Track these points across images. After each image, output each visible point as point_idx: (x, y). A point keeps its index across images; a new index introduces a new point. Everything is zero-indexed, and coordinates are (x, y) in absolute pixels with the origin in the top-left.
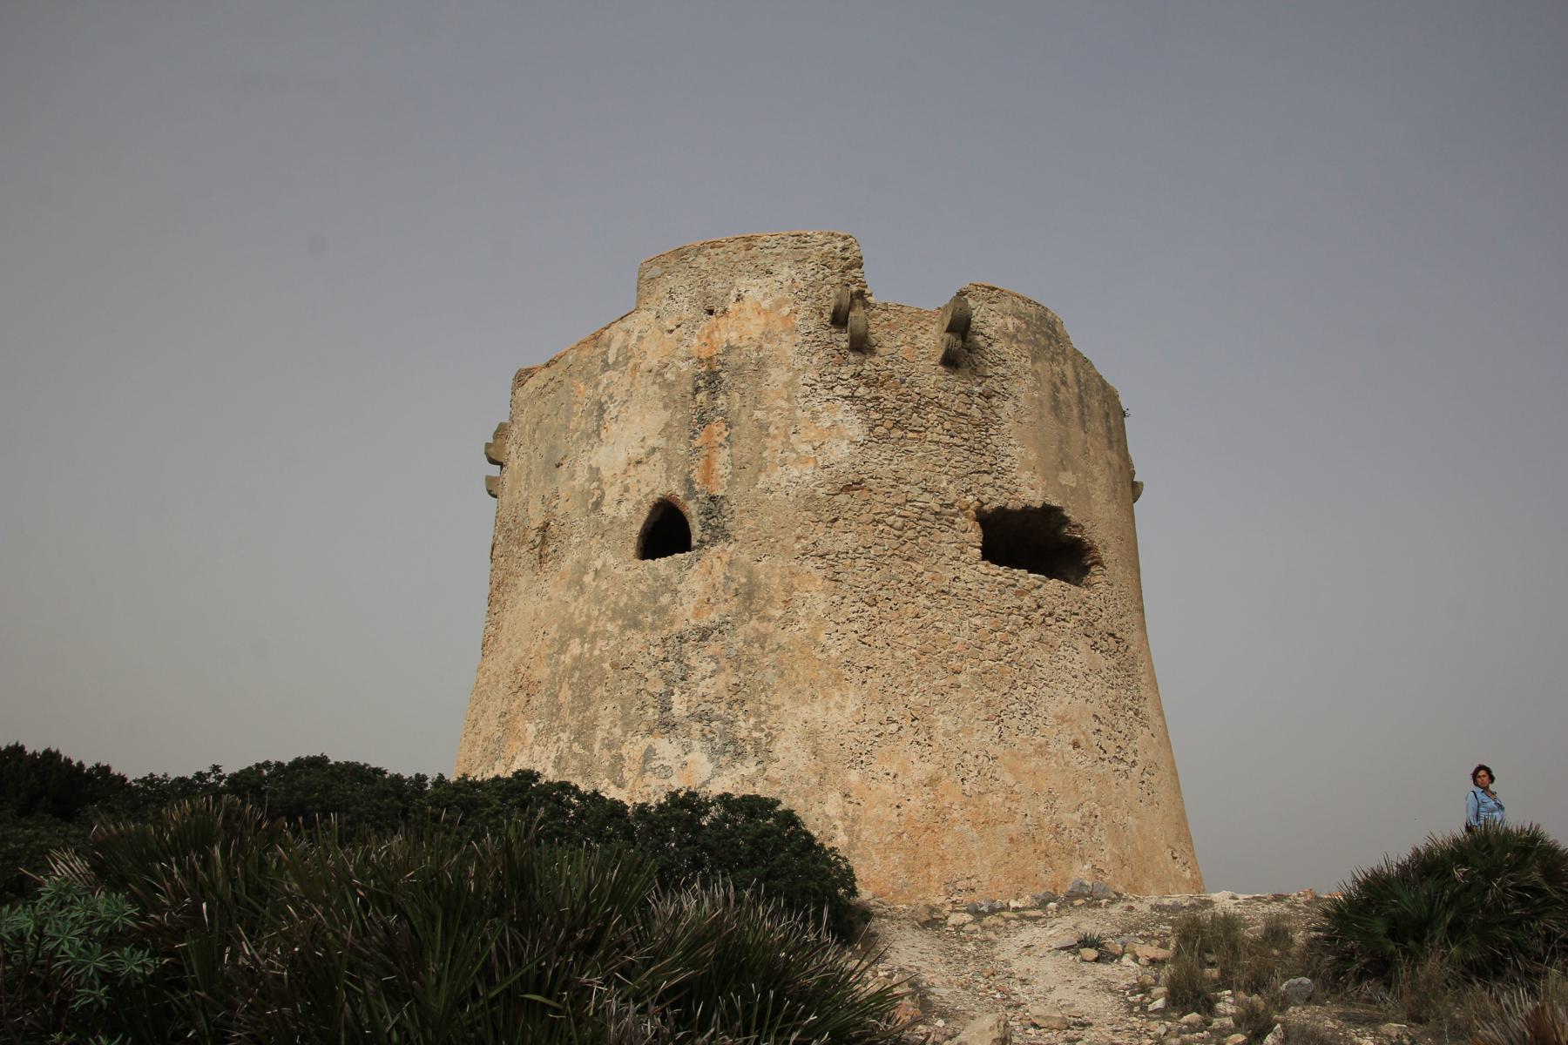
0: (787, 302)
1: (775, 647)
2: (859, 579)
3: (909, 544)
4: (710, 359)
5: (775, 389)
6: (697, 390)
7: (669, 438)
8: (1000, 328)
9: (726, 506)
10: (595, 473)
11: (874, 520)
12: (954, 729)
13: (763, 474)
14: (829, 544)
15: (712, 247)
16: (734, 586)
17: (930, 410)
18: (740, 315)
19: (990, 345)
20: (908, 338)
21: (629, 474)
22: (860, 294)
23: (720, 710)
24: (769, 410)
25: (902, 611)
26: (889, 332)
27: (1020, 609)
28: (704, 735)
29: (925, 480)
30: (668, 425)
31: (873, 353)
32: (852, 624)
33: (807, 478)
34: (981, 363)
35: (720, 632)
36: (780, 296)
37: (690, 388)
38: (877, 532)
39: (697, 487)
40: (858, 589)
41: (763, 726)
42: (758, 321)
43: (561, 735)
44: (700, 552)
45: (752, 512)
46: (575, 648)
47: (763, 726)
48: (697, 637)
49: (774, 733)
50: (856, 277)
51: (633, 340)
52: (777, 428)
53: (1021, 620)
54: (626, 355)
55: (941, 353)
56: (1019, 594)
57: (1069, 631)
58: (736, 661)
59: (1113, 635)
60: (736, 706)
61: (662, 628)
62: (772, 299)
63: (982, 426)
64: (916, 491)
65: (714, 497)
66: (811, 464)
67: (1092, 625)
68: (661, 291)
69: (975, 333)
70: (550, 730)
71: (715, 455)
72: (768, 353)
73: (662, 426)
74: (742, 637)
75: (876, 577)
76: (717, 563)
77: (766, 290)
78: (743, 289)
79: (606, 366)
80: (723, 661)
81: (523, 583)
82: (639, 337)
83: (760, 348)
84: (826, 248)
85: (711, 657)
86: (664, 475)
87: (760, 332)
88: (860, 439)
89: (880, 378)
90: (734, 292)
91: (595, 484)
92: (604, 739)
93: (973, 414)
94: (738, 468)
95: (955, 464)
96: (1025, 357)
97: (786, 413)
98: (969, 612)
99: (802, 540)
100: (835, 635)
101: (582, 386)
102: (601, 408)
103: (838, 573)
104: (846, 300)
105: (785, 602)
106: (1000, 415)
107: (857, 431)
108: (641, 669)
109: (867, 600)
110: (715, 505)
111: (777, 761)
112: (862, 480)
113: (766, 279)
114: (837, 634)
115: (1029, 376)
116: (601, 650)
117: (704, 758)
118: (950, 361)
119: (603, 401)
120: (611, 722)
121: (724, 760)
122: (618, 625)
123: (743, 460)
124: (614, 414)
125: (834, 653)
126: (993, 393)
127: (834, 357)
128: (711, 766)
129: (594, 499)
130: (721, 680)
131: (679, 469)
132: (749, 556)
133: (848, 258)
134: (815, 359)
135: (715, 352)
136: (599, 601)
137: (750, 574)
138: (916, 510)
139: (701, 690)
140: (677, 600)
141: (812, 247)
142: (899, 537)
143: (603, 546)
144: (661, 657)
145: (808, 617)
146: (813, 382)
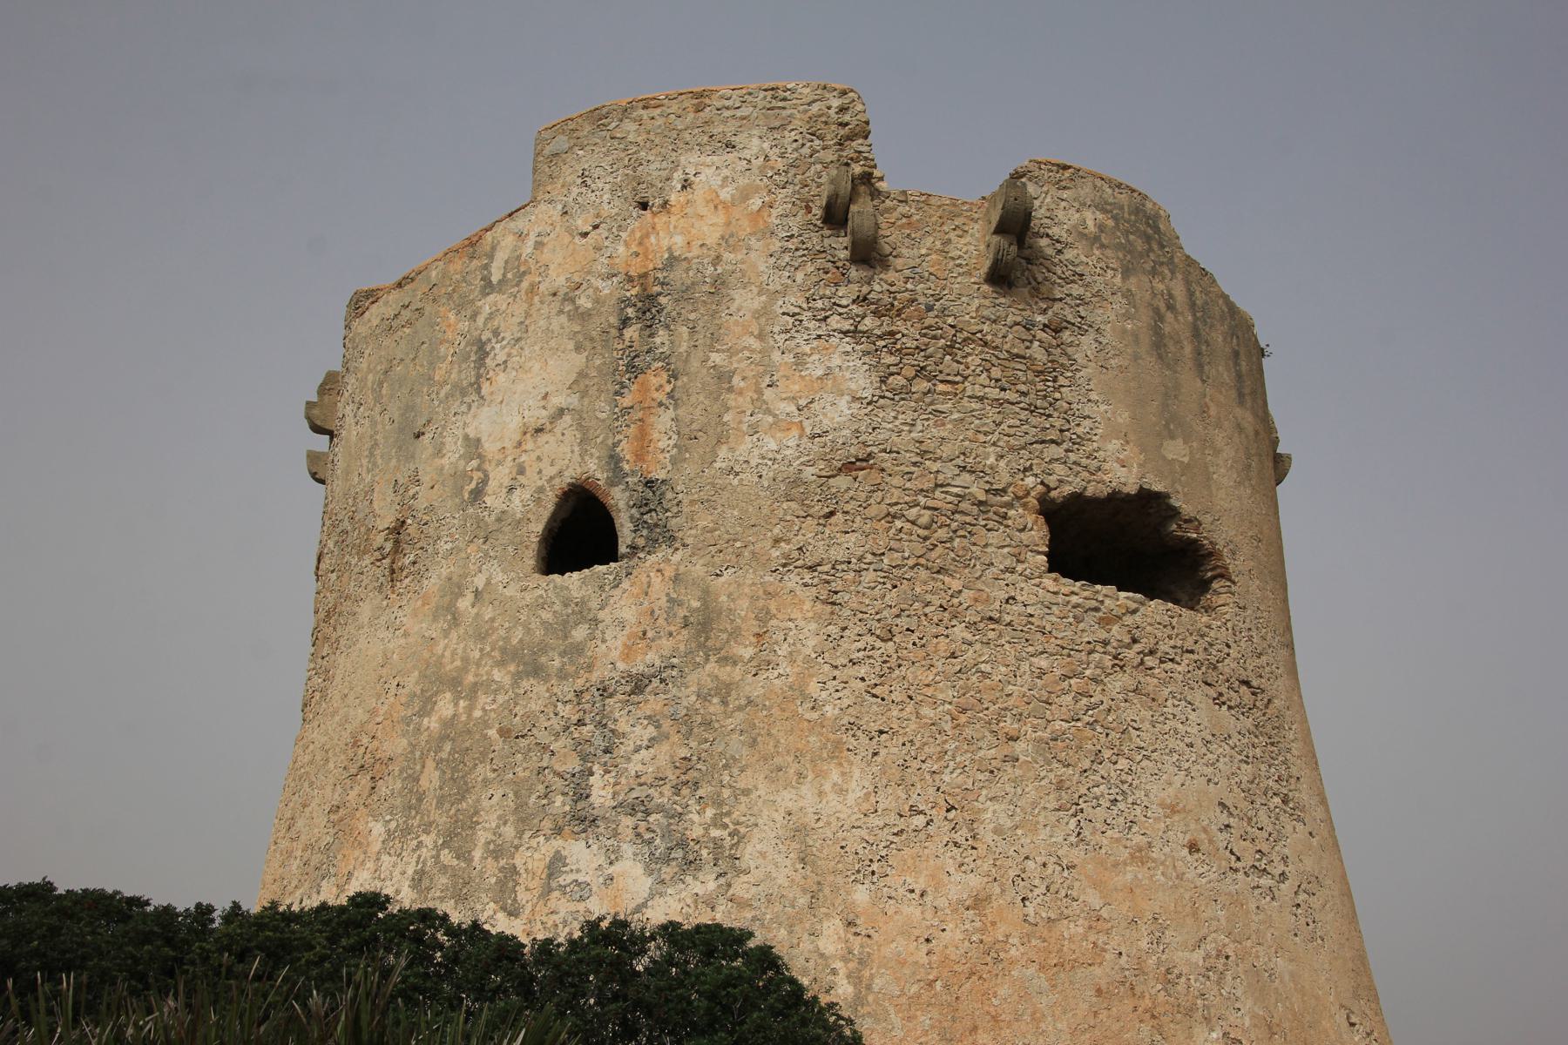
0: (757, 190)
3: (939, 550)
4: (645, 276)
5: (741, 320)
7: (584, 394)
8: (1074, 226)
9: (669, 495)
10: (473, 446)
12: (1009, 824)
13: (724, 447)
15: (645, 107)
16: (682, 612)
18: (687, 210)
19: (1060, 252)
20: (938, 243)
21: (524, 447)
22: (867, 178)
23: (663, 796)
24: (732, 352)
25: (930, 648)
28: (638, 835)
29: (964, 454)
30: (582, 375)
31: (886, 266)
32: (856, 667)
33: (788, 452)
34: (1046, 279)
36: (747, 181)
37: (614, 320)
38: (893, 531)
39: (626, 467)
40: (865, 616)
41: (726, 820)
42: (715, 220)
46: (445, 706)
47: (726, 820)
48: (628, 689)
49: (743, 830)
50: (860, 152)
51: (528, 248)
53: (1108, 661)
54: (518, 270)
55: (987, 264)
56: (1105, 622)
58: (686, 724)
59: (1247, 683)
60: (685, 791)
61: (576, 675)
62: (735, 185)
65: (653, 482)
66: (795, 432)
68: (569, 174)
69: (1038, 235)
70: (406, 831)
72: (729, 267)
73: (573, 377)
74: (695, 688)
75: (892, 596)
76: (657, 580)
77: (726, 172)
79: (488, 287)
80: (666, 725)
84: (815, 108)
86: (576, 449)
87: (718, 235)
88: (867, 394)
89: (896, 303)
90: (678, 176)
92: (489, 843)
94: (687, 438)
95: (1008, 430)
96: (1113, 269)
97: (757, 357)
98: (1030, 649)
101: (452, 316)
103: (836, 593)
104: (846, 187)
105: (758, 635)
106: (1076, 357)
107: (862, 381)
108: (544, 737)
109: (878, 632)
110: (654, 492)
112: (869, 455)
113: (726, 157)
116: (484, 709)
117: (639, 869)
118: (1000, 277)
119: (484, 338)
120: (499, 818)
121: (668, 871)
122: (510, 671)
123: (694, 426)
124: (501, 357)
126: (1065, 324)
129: (473, 485)
130: (663, 752)
131: (599, 440)
134: (800, 276)
135: (651, 266)
136: (481, 637)
137: (706, 595)
138: (950, 498)
139: (634, 767)
141: (795, 107)
142: (926, 538)
143: (486, 555)
144: (574, 719)
145: (792, 660)
146: (797, 310)
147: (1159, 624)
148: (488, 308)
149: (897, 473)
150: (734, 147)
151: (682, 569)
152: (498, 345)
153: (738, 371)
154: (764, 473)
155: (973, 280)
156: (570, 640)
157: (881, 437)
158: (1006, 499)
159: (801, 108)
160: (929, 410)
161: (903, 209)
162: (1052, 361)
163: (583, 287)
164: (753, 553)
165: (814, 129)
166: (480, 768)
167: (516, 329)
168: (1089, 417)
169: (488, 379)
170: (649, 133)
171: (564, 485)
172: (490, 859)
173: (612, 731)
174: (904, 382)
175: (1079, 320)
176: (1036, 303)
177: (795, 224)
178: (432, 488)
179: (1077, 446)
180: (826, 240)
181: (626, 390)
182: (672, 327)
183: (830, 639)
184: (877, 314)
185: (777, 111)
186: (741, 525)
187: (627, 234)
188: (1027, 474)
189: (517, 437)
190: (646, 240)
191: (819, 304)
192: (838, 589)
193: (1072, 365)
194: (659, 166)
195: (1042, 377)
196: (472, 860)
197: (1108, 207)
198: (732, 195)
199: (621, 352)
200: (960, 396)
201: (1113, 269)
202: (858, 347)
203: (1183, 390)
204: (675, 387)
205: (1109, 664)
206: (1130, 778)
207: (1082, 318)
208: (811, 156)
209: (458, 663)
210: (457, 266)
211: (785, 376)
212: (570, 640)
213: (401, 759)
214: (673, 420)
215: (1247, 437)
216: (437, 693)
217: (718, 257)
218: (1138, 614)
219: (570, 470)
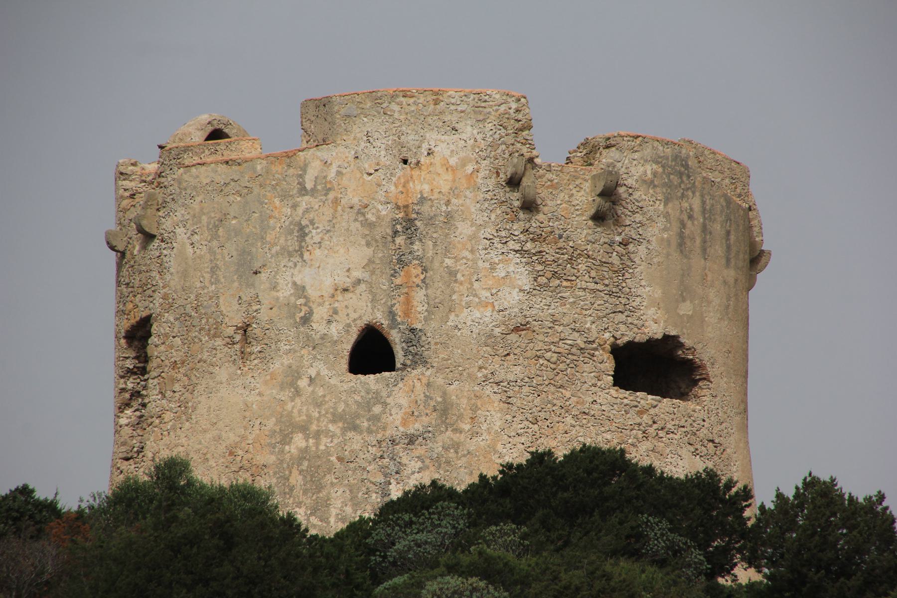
0: (470, 161)
1: (466, 452)
2: (525, 403)
3: (560, 375)
4: (406, 207)
5: (461, 240)
6: (396, 233)
7: (373, 273)
8: (640, 177)
9: (424, 338)
10: (300, 290)
11: (536, 355)
13: (453, 314)
14: (503, 374)
15: (404, 96)
16: (432, 403)
17: (580, 262)
18: (431, 169)
19: (631, 194)
20: (566, 196)
21: (336, 298)
22: (531, 160)
24: (456, 258)
25: (555, 429)
27: (640, 425)
29: (575, 322)
30: (371, 261)
31: (538, 211)
32: (520, 437)
33: (486, 319)
34: (623, 213)
35: (424, 439)
36: (464, 154)
37: (389, 231)
39: (399, 319)
40: (524, 411)
42: (446, 177)
44: (403, 374)
45: (445, 345)
46: (299, 441)
48: (406, 442)
50: (527, 140)
51: (332, 174)
53: (640, 435)
55: (592, 211)
56: (640, 413)
57: (676, 442)
59: (712, 441)
61: (377, 432)
62: (458, 156)
63: (620, 272)
64: (567, 331)
65: (414, 329)
66: (490, 308)
67: (695, 434)
71: (413, 294)
72: (455, 208)
73: (366, 261)
74: (441, 444)
75: (537, 401)
76: (418, 384)
77: (452, 147)
78: (433, 143)
79: (303, 191)
80: (427, 461)
81: (222, 374)
83: (448, 203)
84: (503, 108)
85: (418, 457)
86: (369, 305)
87: (449, 187)
88: (527, 288)
89: (543, 234)
90: (425, 146)
91: (302, 301)
92: (338, 515)
93: (614, 262)
94: (433, 307)
95: (598, 307)
96: (659, 200)
97: (470, 263)
98: (603, 429)
99: (483, 370)
100: (508, 446)
101: (277, 201)
102: (303, 233)
103: (510, 397)
104: (521, 169)
106: (635, 260)
107: (524, 280)
109: (530, 419)
110: (414, 335)
112: (528, 322)
113: (452, 137)
114: (510, 445)
115: (662, 219)
116: (326, 445)
118: (599, 218)
120: (342, 502)
122: (339, 427)
123: (437, 301)
124: (317, 239)
126: (631, 240)
127: (507, 215)
129: (302, 314)
131: (382, 302)
132: (444, 381)
133: (520, 121)
135: (410, 201)
136: (319, 405)
137: (444, 394)
138: (567, 347)
141: (491, 106)
142: (554, 369)
143: (315, 357)
144: (379, 455)
145: (489, 431)
146: (491, 237)
147: (668, 413)
148: (304, 204)
149: (541, 333)
150: (456, 130)
151: (431, 379)
152: (314, 231)
153: (460, 271)
154: (474, 330)
155: (584, 219)
156: (372, 413)
157: (533, 313)
158: (594, 346)
159: (495, 108)
160: (558, 297)
161: (549, 176)
162: (622, 264)
163: (369, 208)
165: (501, 122)
166: (328, 476)
167: (326, 224)
168: (640, 296)
169: (308, 250)
171: (363, 325)
172: (340, 523)
173: (399, 463)
174: (546, 281)
175: (639, 236)
176: (616, 229)
177: (492, 182)
178: (271, 309)
179: (632, 313)
180: (507, 194)
181: (397, 274)
182: (423, 241)
183: (508, 422)
184: (533, 240)
185: (480, 109)
186: (462, 358)
187: (396, 178)
188: (606, 331)
190: (407, 185)
191: (503, 234)
192: (511, 396)
193: (633, 265)
194: (413, 138)
195: (617, 275)
196: (330, 522)
197: (660, 160)
198: (456, 163)
199: (394, 251)
200: (574, 288)
201: (659, 200)
202: (524, 260)
203: (693, 269)
204: (426, 277)
205: (641, 436)
207: (640, 235)
208: (499, 140)
209: (304, 418)
210: (277, 168)
211: (485, 276)
212: (372, 413)
213: (274, 466)
214: (425, 295)
215: (729, 286)
216: (292, 433)
217: (448, 201)
218: (657, 407)
219: (366, 316)
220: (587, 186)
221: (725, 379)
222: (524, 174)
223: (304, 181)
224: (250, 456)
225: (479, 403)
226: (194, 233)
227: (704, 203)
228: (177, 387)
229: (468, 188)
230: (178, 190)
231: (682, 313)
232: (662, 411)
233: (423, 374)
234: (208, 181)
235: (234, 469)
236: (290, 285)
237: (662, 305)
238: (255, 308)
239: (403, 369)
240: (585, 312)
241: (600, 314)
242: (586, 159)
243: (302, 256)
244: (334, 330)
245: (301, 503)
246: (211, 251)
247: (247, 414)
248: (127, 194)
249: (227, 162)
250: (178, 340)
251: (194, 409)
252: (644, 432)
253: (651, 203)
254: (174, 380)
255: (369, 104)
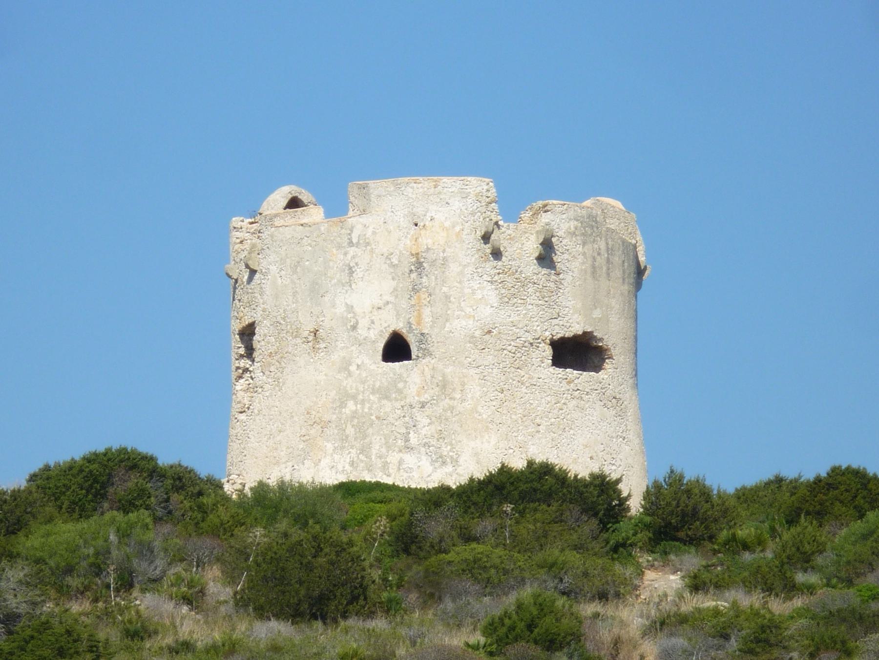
0: (458, 223)
2: (495, 379)
4: (418, 254)
6: (411, 271)
7: (396, 297)
8: (567, 230)
9: (430, 339)
10: (350, 308)
12: (537, 452)
13: (448, 323)
15: (415, 183)
16: (436, 381)
20: (520, 245)
23: (433, 442)
25: (515, 396)
26: (510, 243)
28: (427, 453)
30: (395, 290)
33: (470, 326)
38: (503, 355)
39: (414, 327)
41: (454, 450)
43: (351, 450)
46: (351, 406)
47: (454, 450)
48: (420, 406)
49: (459, 453)
52: (455, 298)
55: (537, 254)
56: (569, 383)
60: (441, 440)
64: (522, 332)
66: (472, 319)
70: (342, 448)
72: (449, 255)
73: (392, 290)
76: (426, 369)
79: (351, 244)
80: (433, 419)
82: (373, 231)
83: (444, 251)
86: (395, 318)
88: (495, 305)
97: (459, 290)
100: (485, 407)
101: (334, 251)
102: (351, 271)
105: (462, 391)
108: (393, 421)
111: (461, 466)
115: (581, 256)
117: (428, 464)
119: (351, 265)
120: (380, 446)
121: (437, 465)
123: (438, 315)
124: (360, 275)
125: (485, 416)
128: (431, 468)
129: (352, 324)
130: (433, 427)
131: (403, 316)
136: (363, 382)
137: (444, 375)
138: (522, 342)
140: (407, 386)
141: (471, 188)
142: (514, 357)
148: (352, 252)
151: (435, 365)
152: (358, 270)
158: (539, 341)
159: (473, 189)
164: (459, 362)
170: (417, 194)
173: (416, 420)
189: (370, 309)
191: (479, 270)
196: (371, 459)
202: (493, 287)
206: (573, 437)
209: (354, 391)
220: (533, 238)
221: (623, 357)
222: (492, 232)
223: (351, 237)
224: (320, 415)
225: (466, 380)
226: (282, 269)
227: (607, 244)
228: (272, 369)
229: (457, 241)
230: (271, 242)
231: (594, 316)
232: (583, 381)
233: (430, 362)
234: (290, 236)
235: (309, 423)
236: (343, 305)
237: (582, 312)
238: (321, 319)
239: (416, 359)
240: (532, 319)
241: (542, 320)
242: (532, 218)
243: (351, 286)
244: (372, 335)
245: (353, 446)
246: (293, 282)
247: (318, 387)
248: (238, 241)
249: (302, 225)
250: (273, 339)
251: (284, 384)
252: (572, 395)
253: (574, 246)
254: (270, 364)
255: (392, 188)
